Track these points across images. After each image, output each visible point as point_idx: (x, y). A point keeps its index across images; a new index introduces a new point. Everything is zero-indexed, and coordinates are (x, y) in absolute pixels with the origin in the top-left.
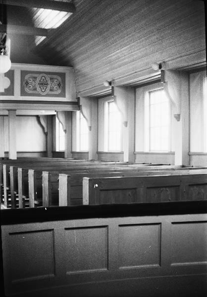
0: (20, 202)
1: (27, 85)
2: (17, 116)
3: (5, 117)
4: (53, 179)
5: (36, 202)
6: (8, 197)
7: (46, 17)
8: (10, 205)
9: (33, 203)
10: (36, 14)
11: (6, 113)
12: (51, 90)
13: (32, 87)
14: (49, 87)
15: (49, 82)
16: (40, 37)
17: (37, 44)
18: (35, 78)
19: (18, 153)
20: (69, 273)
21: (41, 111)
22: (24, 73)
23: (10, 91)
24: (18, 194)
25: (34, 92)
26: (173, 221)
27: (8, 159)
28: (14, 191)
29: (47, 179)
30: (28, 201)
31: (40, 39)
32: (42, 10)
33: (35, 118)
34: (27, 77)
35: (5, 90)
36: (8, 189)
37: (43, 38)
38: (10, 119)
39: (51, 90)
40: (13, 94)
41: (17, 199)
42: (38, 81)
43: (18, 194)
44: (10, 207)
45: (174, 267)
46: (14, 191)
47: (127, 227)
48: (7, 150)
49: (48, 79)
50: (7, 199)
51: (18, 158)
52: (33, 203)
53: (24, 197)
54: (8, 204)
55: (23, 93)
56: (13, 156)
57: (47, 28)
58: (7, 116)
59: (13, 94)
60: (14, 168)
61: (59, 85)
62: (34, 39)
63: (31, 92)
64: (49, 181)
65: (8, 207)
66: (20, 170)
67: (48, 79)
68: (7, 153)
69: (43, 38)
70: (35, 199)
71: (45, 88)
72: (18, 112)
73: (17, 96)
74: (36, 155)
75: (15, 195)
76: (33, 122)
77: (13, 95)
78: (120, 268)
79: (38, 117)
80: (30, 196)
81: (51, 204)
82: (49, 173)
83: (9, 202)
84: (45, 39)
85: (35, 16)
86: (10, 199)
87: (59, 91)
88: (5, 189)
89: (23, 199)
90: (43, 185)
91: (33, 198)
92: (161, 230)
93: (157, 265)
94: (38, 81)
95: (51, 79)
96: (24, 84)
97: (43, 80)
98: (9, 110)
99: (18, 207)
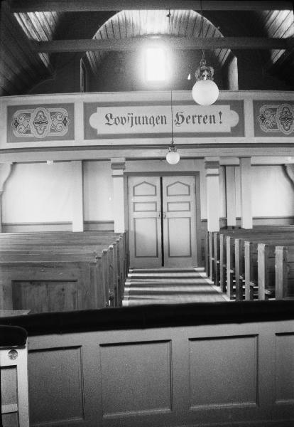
0: (246, 290)
1: (263, 120)
2: (252, 165)
3: (236, 167)
4: (253, 257)
5: (267, 292)
6: (233, 284)
7: (283, 21)
8: (235, 296)
9: (263, 292)
10: (269, 18)
11: (237, 161)
12: (52, 130)
13: (23, 128)
14: (49, 126)
15: (49, 119)
16: (277, 51)
17: (275, 60)
18: (29, 115)
19: (254, 219)
20: (105, 416)
21: (286, 158)
22: (257, 104)
23: (238, 130)
24: (244, 279)
25: (275, 131)
26: (101, 343)
27: (240, 228)
28: (241, 274)
29: (282, 255)
30: (257, 289)
31: (278, 54)
32: (276, 12)
33: (280, 168)
34: (16, 115)
35: (232, 129)
36: (232, 271)
37: (282, 51)
38: (242, 169)
39: (52, 130)
40: (243, 135)
41: (244, 287)
42: (32, 120)
43: (244, 279)
44: (234, 298)
45: (194, 412)
46: (241, 274)
47: (67, 351)
48: (239, 216)
49: (47, 115)
50: (231, 287)
51: (254, 226)
52: (263, 292)
53: (252, 284)
54: (231, 294)
55: (258, 132)
56: (247, 225)
57: (285, 37)
58: (238, 165)
59: (243, 135)
60: (240, 241)
61: (65, 122)
62: (269, 55)
63: (268, 131)
64: (284, 260)
65: (231, 298)
66: (261, 248)
67: (47, 115)
68: (239, 219)
69: (282, 51)
70: (266, 288)
71: (42, 128)
72: (254, 161)
73: (250, 137)
74: (282, 223)
75: (241, 280)
76: (277, 175)
77: (73, 139)
78: (192, 407)
79: (284, 167)
80: (259, 282)
81: (286, 294)
82: (284, 249)
83: (233, 291)
84: (283, 55)
85: (269, 22)
86: (234, 287)
87: (65, 131)
88: (229, 271)
89: (251, 287)
90: (276, 266)
91: (264, 285)
92: (171, 348)
93: (166, 410)
94: (32, 120)
95: (52, 114)
96: (259, 118)
97: (40, 116)
98: (240, 158)
99: (244, 298)
